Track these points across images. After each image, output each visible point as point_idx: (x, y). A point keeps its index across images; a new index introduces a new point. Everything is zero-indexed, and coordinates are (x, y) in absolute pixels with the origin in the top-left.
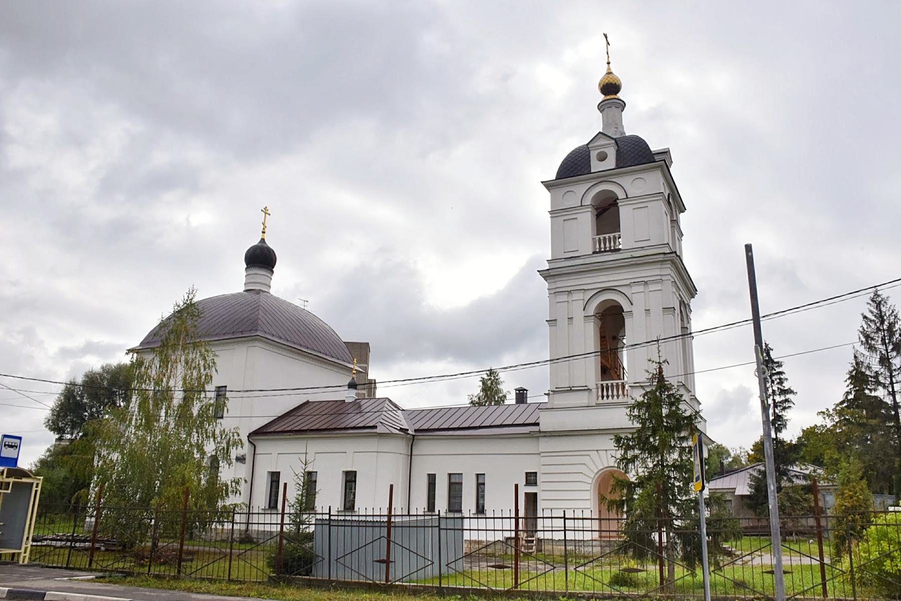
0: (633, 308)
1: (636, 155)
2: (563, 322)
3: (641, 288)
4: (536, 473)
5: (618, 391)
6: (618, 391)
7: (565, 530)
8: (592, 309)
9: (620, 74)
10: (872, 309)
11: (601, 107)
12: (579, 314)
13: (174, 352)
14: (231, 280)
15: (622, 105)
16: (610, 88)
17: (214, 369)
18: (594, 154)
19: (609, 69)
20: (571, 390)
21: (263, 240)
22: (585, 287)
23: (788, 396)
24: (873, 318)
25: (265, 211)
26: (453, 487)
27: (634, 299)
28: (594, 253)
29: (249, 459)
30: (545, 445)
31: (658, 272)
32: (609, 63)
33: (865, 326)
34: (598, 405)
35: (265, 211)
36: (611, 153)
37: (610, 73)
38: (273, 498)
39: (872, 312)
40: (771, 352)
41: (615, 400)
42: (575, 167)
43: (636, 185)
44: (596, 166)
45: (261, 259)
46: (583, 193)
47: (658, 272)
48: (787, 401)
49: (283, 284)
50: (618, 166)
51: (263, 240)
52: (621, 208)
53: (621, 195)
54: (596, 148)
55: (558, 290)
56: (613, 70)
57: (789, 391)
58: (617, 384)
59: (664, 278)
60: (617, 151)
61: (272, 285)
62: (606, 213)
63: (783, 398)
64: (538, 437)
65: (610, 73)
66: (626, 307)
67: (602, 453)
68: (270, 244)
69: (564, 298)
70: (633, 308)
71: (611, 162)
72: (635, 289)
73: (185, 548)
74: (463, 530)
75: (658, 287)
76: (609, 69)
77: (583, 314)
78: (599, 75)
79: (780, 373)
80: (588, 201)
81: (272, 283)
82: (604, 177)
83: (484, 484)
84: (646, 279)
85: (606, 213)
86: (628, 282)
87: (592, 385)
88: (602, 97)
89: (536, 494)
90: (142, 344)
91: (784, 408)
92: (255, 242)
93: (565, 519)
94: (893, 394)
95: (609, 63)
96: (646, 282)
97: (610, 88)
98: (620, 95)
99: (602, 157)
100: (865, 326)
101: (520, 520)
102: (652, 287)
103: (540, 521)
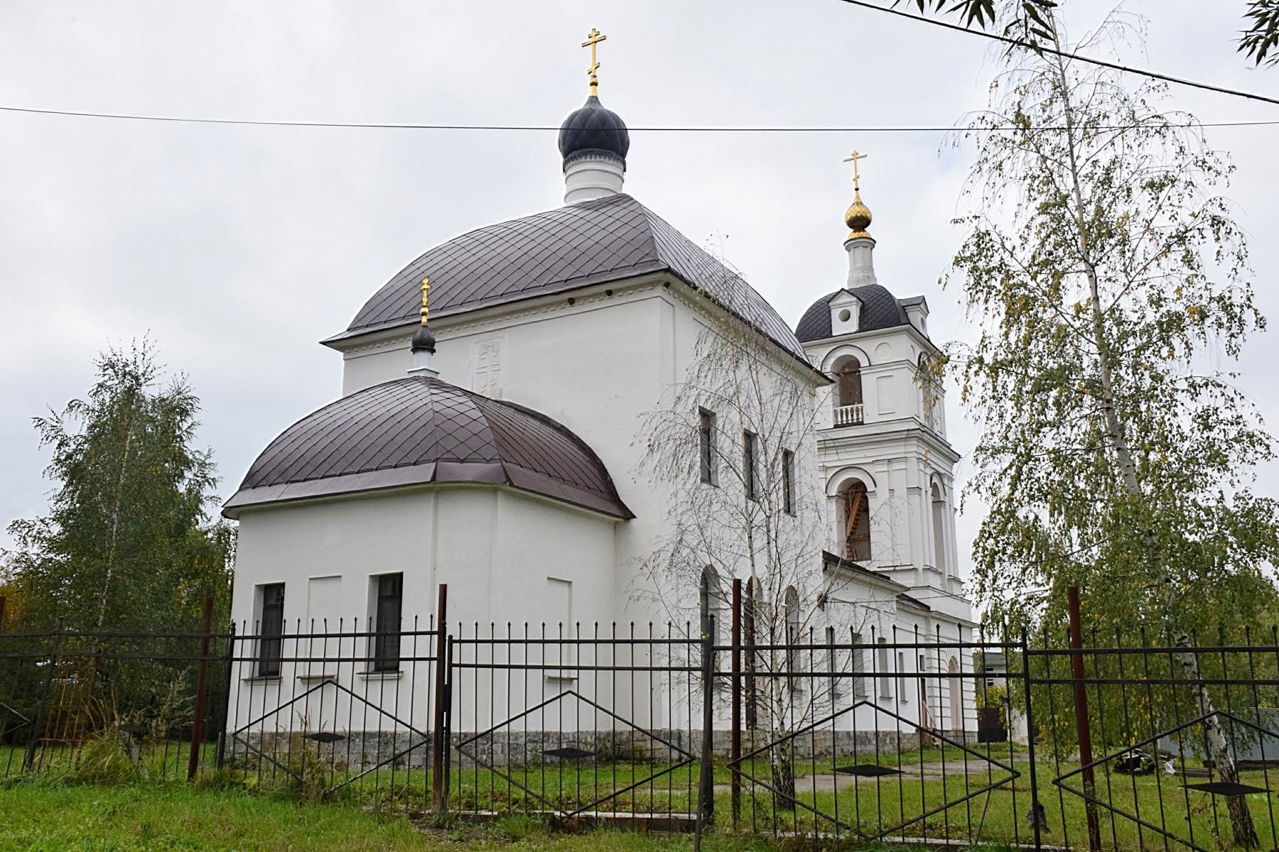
4: (400, 576)
7: (833, 675)
8: (834, 491)
11: (850, 245)
14: (545, 188)
15: (873, 243)
16: (859, 223)
18: (836, 314)
21: (594, 100)
28: (836, 426)
36: (855, 312)
44: (839, 328)
49: (647, 177)
50: (861, 329)
51: (594, 100)
52: (863, 378)
53: (864, 363)
54: (840, 305)
60: (862, 309)
65: (859, 203)
68: (609, 104)
71: (853, 325)
73: (784, 670)
74: (441, 739)
78: (845, 210)
82: (847, 340)
88: (849, 233)
92: (580, 105)
93: (790, 675)
97: (859, 223)
99: (846, 317)
101: (743, 678)
102: (896, 466)
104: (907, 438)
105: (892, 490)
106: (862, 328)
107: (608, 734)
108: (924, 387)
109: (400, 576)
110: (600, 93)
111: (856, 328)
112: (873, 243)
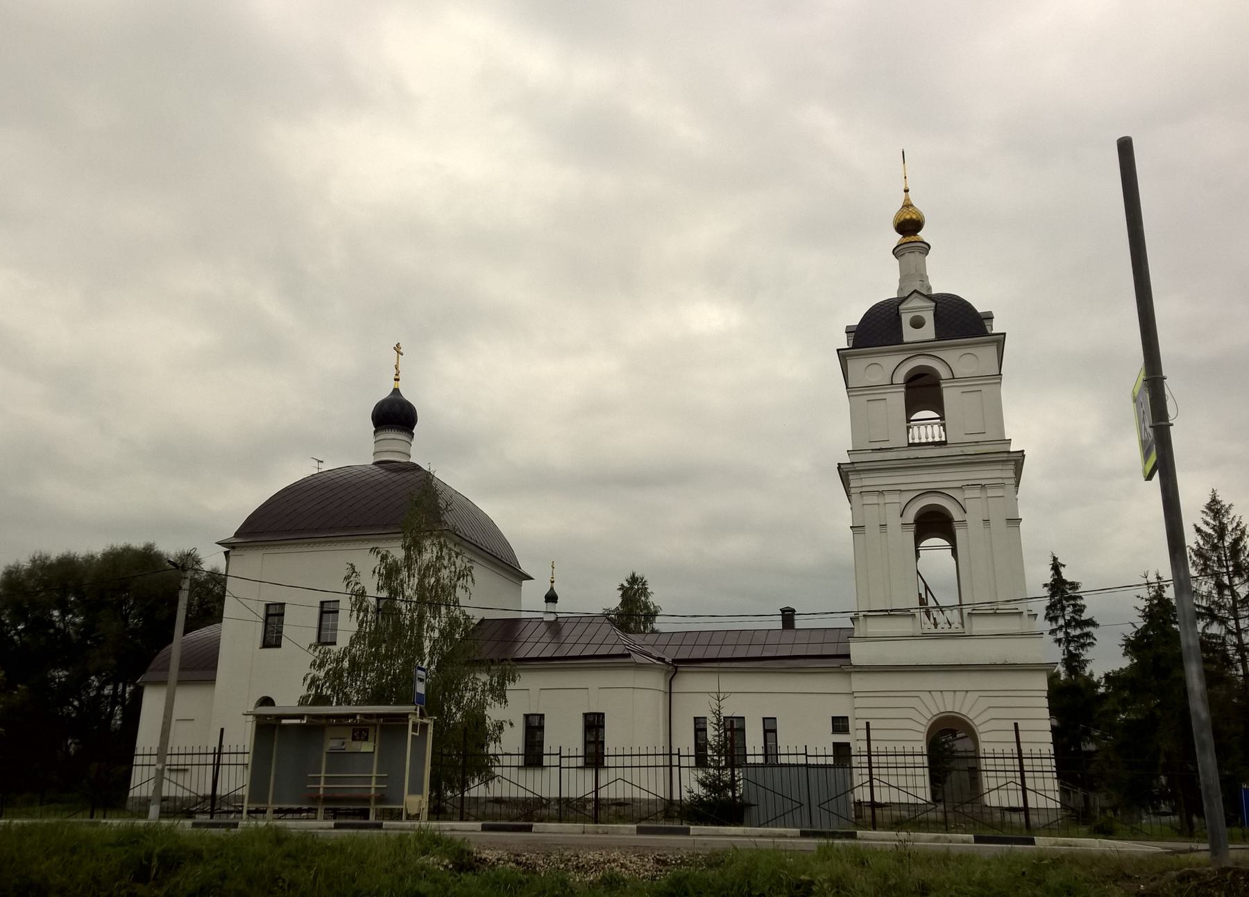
0: (967, 517)
1: (961, 321)
2: (872, 530)
3: (976, 493)
4: (834, 719)
8: (911, 516)
9: (922, 205)
10: (1208, 519)
11: (897, 252)
12: (894, 521)
13: (420, 552)
14: (358, 449)
15: (926, 248)
16: (909, 226)
17: (469, 578)
18: (906, 319)
19: (907, 199)
20: (889, 614)
21: (396, 391)
23: (1087, 630)
24: (1210, 531)
25: (397, 348)
26: (769, 735)
27: (968, 505)
30: (859, 683)
31: (997, 474)
32: (906, 191)
33: (1201, 542)
36: (929, 317)
39: (1207, 524)
40: (1062, 569)
42: (877, 330)
43: (958, 361)
44: (909, 334)
46: (887, 367)
47: (997, 474)
48: (1088, 635)
51: (396, 391)
53: (944, 373)
57: (1090, 622)
59: (1006, 482)
62: (923, 391)
63: (1078, 632)
64: (850, 673)
66: (956, 514)
67: (937, 695)
68: (407, 395)
69: (873, 499)
70: (967, 517)
72: (969, 493)
75: (999, 492)
76: (907, 199)
77: (901, 521)
78: (892, 210)
79: (1075, 598)
80: (900, 378)
81: (413, 451)
82: (921, 348)
83: (775, 731)
84: (983, 482)
85: (923, 391)
88: (898, 237)
89: (848, 744)
90: (237, 535)
91: (1083, 646)
92: (385, 393)
94: (1239, 632)
95: (906, 191)
96: (983, 486)
97: (909, 226)
98: (922, 234)
99: (917, 323)
100: (1201, 542)
102: (991, 493)
103: (983, 761)
106: (941, 335)
107: (205, 798)
108: (606, 615)
109: (834, 719)
110: (402, 386)
111: (933, 336)
112: (926, 248)
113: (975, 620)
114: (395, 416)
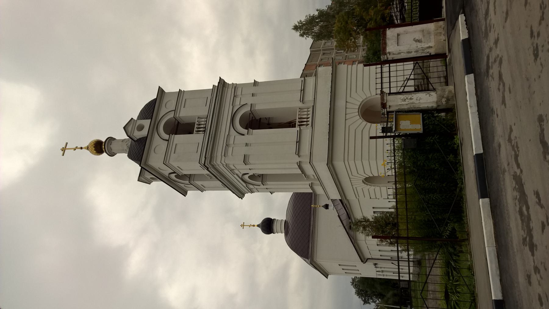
5: (304, 122)
6: (304, 122)
8: (245, 131)
11: (112, 154)
14: (279, 239)
16: (99, 147)
19: (85, 148)
21: (258, 226)
22: (227, 133)
25: (243, 226)
29: (375, 262)
34: (312, 126)
35: (243, 226)
37: (88, 148)
38: (338, 184)
41: (310, 119)
43: (166, 113)
45: (268, 226)
51: (258, 226)
55: (223, 154)
56: (86, 145)
58: (299, 122)
61: (208, 83)
67: (348, 116)
68: (259, 222)
76: (85, 148)
78: (88, 155)
80: (166, 137)
81: (280, 219)
86: (231, 107)
87: (310, 182)
92: (259, 230)
97: (99, 147)
98: (104, 140)
104: (213, 166)
105: (253, 95)
113: (306, 99)
114: (268, 226)
